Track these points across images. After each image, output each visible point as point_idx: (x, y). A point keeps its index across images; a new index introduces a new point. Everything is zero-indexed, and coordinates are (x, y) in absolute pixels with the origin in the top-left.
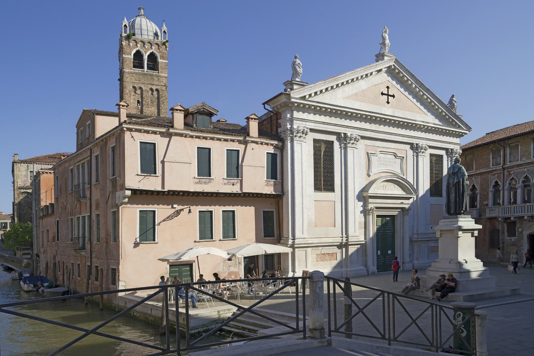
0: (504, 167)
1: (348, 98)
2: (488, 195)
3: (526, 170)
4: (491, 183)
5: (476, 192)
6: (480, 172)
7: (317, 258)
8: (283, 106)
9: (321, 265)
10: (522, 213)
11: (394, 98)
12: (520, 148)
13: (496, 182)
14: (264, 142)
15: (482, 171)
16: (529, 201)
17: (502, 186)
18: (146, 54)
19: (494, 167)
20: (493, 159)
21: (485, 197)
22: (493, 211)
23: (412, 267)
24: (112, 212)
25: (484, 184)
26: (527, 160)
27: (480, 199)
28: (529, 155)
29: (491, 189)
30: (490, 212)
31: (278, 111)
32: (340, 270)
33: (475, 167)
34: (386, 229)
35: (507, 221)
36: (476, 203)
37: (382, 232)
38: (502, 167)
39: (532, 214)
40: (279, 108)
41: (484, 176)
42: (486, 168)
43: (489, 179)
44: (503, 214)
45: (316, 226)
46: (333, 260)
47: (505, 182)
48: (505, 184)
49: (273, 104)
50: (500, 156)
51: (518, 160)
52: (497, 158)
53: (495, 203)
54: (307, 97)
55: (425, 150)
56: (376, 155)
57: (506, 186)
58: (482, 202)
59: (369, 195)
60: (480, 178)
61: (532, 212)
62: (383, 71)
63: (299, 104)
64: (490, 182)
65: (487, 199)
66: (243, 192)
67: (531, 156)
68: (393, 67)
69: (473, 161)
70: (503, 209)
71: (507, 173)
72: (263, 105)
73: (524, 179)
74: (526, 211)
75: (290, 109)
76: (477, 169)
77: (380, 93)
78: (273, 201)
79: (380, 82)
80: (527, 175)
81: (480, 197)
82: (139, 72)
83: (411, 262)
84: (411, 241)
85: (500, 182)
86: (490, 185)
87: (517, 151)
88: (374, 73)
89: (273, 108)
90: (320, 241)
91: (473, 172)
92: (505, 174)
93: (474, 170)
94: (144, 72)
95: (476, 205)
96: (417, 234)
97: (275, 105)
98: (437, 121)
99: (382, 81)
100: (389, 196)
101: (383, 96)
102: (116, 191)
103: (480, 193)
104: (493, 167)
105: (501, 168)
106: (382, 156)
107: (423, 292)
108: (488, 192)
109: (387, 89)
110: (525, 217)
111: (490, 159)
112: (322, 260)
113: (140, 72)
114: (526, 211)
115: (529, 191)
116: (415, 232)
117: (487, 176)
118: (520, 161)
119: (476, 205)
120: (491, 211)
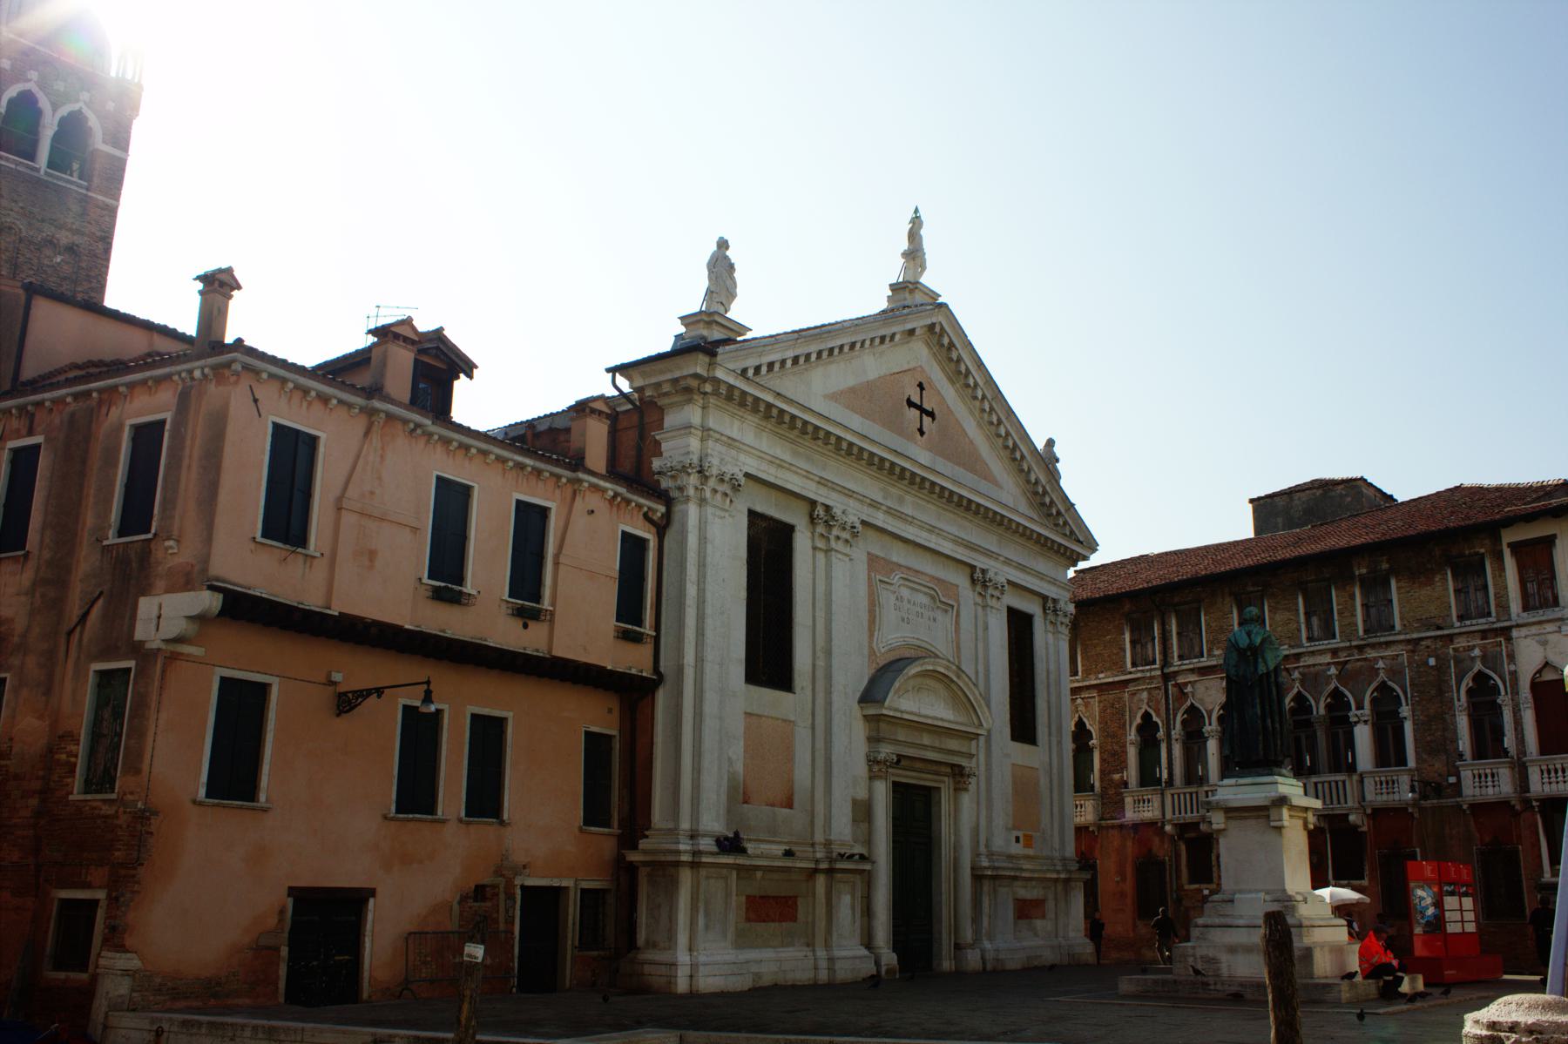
0: (1166, 671)
2: (1125, 752)
5: (1090, 743)
6: (1098, 682)
12: (1206, 621)
13: (1080, 724)
15: (1104, 678)
17: (1163, 728)
18: (54, 111)
20: (1135, 647)
21: (1115, 760)
22: (1144, 803)
23: (981, 961)
24: (95, 671)
25: (1111, 721)
27: (1101, 766)
29: (1132, 735)
30: (1136, 805)
31: (656, 400)
33: (1083, 666)
35: (1186, 836)
38: (1162, 672)
41: (1111, 695)
43: (1126, 705)
44: (1177, 812)
47: (1172, 717)
48: (1172, 722)
49: (644, 375)
50: (1154, 639)
51: (1202, 656)
52: (1146, 643)
53: (1148, 777)
54: (750, 373)
56: (892, 588)
57: (1174, 729)
58: (1109, 773)
59: (885, 712)
62: (917, 334)
63: (731, 387)
65: (1123, 766)
66: (553, 654)
68: (937, 329)
70: (1176, 796)
71: (1175, 689)
72: (611, 374)
76: (1087, 673)
77: (906, 398)
79: (906, 367)
81: (1103, 760)
82: (18, 168)
84: (978, 878)
85: (1158, 715)
86: (1128, 722)
88: (897, 337)
91: (1078, 681)
92: (1170, 692)
93: (1080, 673)
94: (36, 174)
98: (1023, 507)
99: (908, 363)
100: (929, 721)
101: (912, 409)
102: (145, 590)
103: (1101, 747)
104: (1134, 669)
105: (1159, 673)
107: (1209, 985)
108: (1125, 746)
109: (918, 389)
111: (1125, 645)
113: (20, 168)
116: (982, 849)
120: (1139, 803)
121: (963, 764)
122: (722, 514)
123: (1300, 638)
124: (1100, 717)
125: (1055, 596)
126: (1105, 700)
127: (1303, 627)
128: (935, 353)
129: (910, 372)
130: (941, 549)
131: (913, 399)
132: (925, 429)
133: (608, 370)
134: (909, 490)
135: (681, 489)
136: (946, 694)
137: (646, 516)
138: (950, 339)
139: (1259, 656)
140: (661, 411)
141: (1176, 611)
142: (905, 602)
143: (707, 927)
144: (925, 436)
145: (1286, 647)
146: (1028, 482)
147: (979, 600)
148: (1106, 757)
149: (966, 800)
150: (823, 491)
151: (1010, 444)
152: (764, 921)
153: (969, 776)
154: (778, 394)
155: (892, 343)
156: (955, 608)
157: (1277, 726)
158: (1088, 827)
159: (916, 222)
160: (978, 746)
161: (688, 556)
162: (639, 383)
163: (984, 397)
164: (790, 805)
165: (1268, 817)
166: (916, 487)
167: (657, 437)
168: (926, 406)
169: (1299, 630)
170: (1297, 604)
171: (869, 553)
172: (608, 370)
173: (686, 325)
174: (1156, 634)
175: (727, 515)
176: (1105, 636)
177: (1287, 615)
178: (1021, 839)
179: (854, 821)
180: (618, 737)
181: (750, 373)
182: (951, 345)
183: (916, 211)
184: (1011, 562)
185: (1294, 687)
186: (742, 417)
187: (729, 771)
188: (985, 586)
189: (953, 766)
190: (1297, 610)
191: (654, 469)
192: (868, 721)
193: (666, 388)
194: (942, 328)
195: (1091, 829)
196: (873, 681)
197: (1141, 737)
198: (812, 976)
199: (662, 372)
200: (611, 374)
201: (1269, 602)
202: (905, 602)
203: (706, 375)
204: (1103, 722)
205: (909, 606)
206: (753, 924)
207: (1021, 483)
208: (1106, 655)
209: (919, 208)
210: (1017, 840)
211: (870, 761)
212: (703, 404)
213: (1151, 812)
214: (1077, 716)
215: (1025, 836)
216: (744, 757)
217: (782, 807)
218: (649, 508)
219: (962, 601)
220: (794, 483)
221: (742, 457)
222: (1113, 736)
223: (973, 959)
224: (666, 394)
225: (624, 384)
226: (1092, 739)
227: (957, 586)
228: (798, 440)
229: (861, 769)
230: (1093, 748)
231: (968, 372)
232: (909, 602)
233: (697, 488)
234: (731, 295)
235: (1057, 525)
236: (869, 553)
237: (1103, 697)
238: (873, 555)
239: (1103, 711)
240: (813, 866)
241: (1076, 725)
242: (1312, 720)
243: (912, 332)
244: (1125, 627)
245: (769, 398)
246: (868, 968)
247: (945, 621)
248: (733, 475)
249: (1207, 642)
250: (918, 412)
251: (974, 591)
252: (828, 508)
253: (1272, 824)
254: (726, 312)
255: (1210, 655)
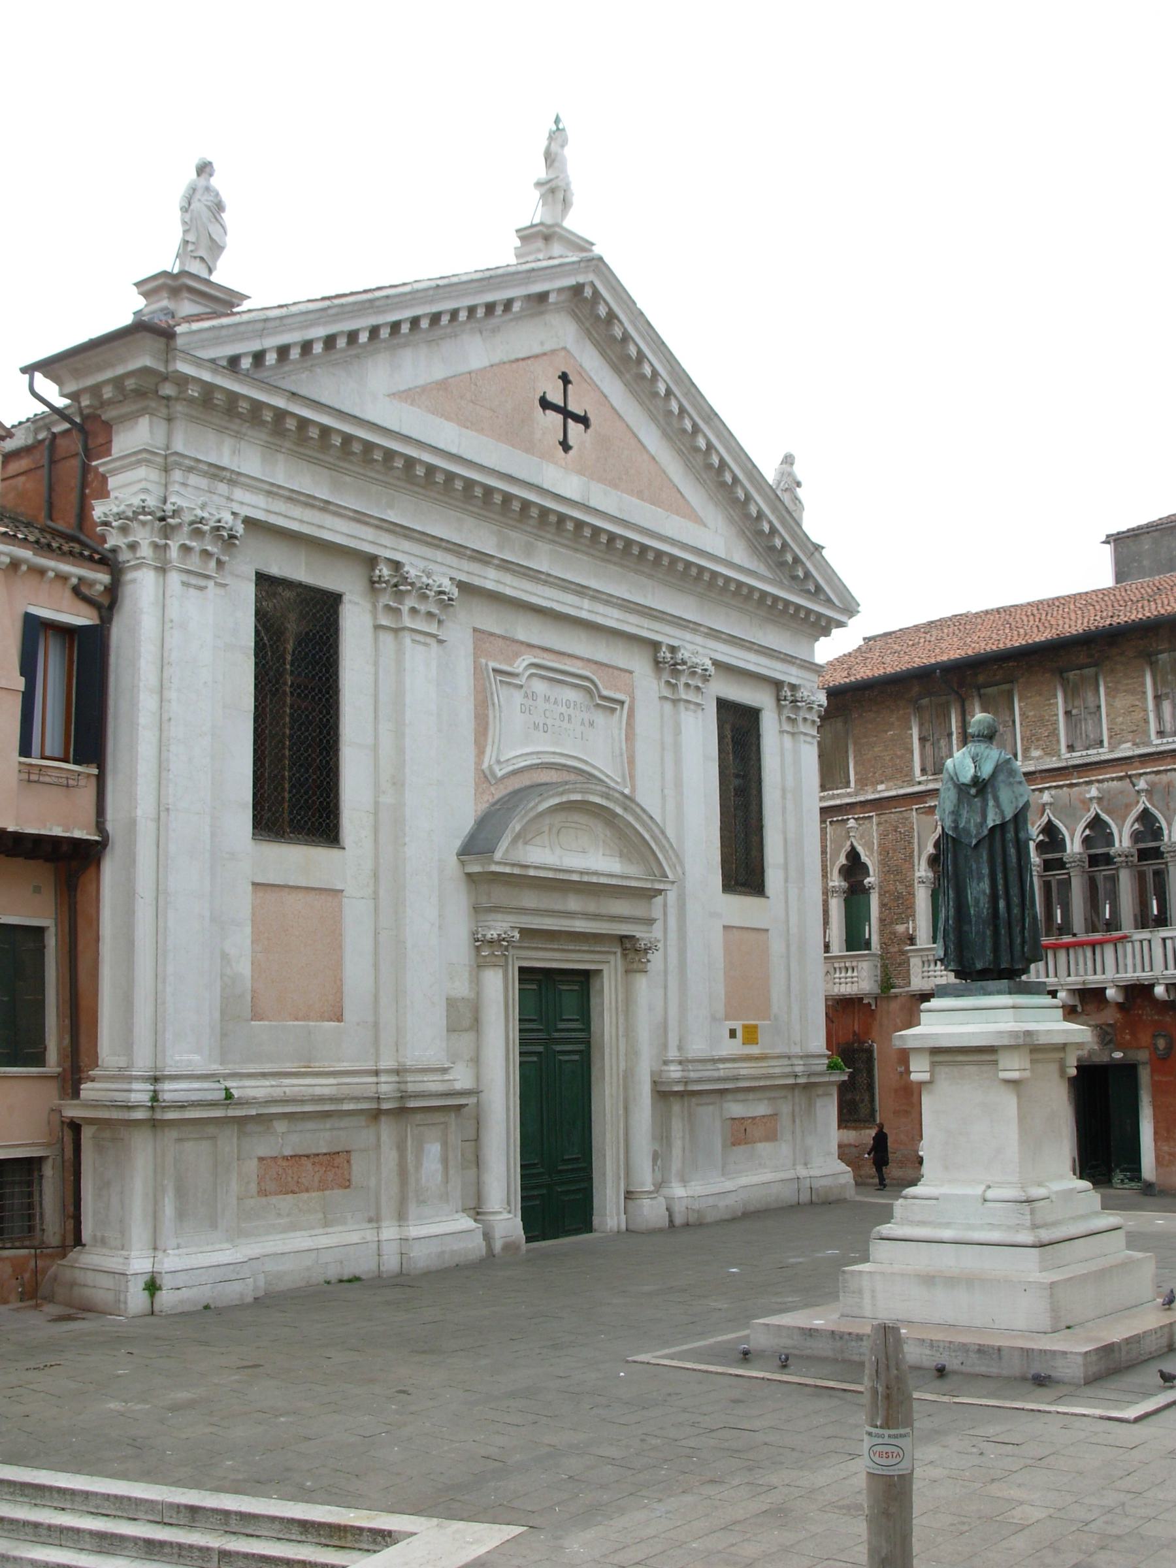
1: (408, 396)
2: (912, 895)
3: (1094, 792)
4: (919, 845)
6: (877, 796)
7: (261, 1179)
8: (132, 390)
9: (279, 1215)
10: (1143, 970)
11: (589, 431)
12: (1020, 708)
14: (26, 561)
15: (884, 790)
16: (1162, 921)
19: (930, 778)
25: (895, 850)
26: (1047, 759)
27: (881, 913)
28: (1050, 738)
31: (99, 412)
32: (370, 1235)
33: (856, 774)
34: (556, 1035)
36: (867, 928)
37: (540, 1049)
39: (1084, 983)
40: (105, 397)
42: (899, 783)
45: (256, 1016)
46: (332, 1189)
49: (77, 374)
50: (950, 735)
52: (939, 740)
54: (246, 363)
55: (706, 678)
58: (892, 923)
59: (495, 868)
60: (879, 824)
61: (1147, 968)
63: (209, 389)
64: (916, 840)
67: (1058, 741)
68: (588, 292)
69: (847, 752)
72: (27, 376)
73: (1087, 832)
74: (1130, 969)
75: (164, 411)
77: (538, 397)
78: (41, 873)
80: (1053, 818)
81: (883, 905)
83: (659, 1186)
86: (916, 853)
87: (1008, 719)
88: (516, 307)
89: (74, 396)
90: (277, 1093)
91: (849, 795)
93: (852, 784)
95: (867, 936)
96: (680, 1063)
97: (90, 381)
98: (740, 555)
99: (542, 344)
101: (548, 412)
103: (880, 887)
104: (924, 778)
106: (539, 687)
108: (912, 886)
109: (560, 382)
110: (1108, 992)
111: (912, 744)
112: (286, 1190)
114: (1130, 969)
115: (1160, 877)
117: (905, 814)
118: (1022, 761)
119: (867, 936)
121: (638, 935)
122: (202, 582)
123: (1146, 733)
124: (880, 845)
125: (794, 681)
126: (886, 821)
127: (1152, 717)
128: (587, 329)
129: (545, 358)
130: (600, 620)
131: (549, 398)
132: (571, 443)
133: (24, 370)
134: (557, 539)
135: (133, 547)
136: (608, 833)
137: (76, 591)
138: (610, 309)
139: (990, 796)
140: (108, 427)
141: (980, 696)
142: (540, 701)
143: (181, 1215)
144: (571, 452)
145: (1129, 745)
146: (747, 516)
147: (667, 693)
148: (886, 900)
149: (643, 986)
150: (386, 539)
151: (715, 460)
152: (293, 1192)
153: (646, 951)
154: (294, 394)
155: (508, 316)
156: (626, 706)
157: (1016, 911)
158: (862, 999)
159: (557, 134)
160: (665, 905)
161: (142, 649)
162: (72, 387)
163: (669, 392)
164: (340, 1019)
165: (995, 1062)
166: (553, 529)
167: (101, 470)
168: (573, 407)
169: (1146, 721)
170: (1143, 684)
171: (475, 630)
172: (24, 370)
173: (146, 295)
174: (954, 729)
175: (211, 584)
176: (886, 731)
177: (1130, 700)
178: (739, 1033)
179: (451, 1030)
180: (52, 930)
181: (246, 363)
182: (612, 316)
183: (557, 121)
184: (719, 635)
185: (1138, 802)
186: (238, 432)
187: (222, 975)
188: (675, 672)
189: (622, 939)
190: (1145, 693)
191: (95, 517)
192: (474, 882)
193: (108, 393)
194: (596, 293)
195: (865, 1001)
196: (482, 823)
197: (935, 873)
198: (374, 1267)
199: (100, 368)
200: (27, 376)
201: (1105, 683)
202: (540, 701)
203: (162, 369)
204: (885, 852)
205: (547, 706)
206: (274, 1200)
207: (736, 518)
208: (888, 758)
209: (561, 116)
210: (733, 1033)
211: (478, 941)
212: (169, 415)
213: (945, 978)
214: (849, 843)
215: (745, 1027)
216: (253, 951)
217: (322, 1018)
218: (80, 579)
219: (638, 694)
220: (337, 531)
221: (239, 494)
222: (897, 871)
223: (651, 1211)
224: (111, 402)
225: (48, 388)
226: (869, 876)
227: (631, 672)
228: (341, 464)
229: (460, 950)
230: (870, 888)
231: (641, 356)
232: (547, 699)
233: (156, 546)
234: (217, 248)
235: (794, 578)
236: (475, 630)
237: (884, 818)
238: (483, 632)
239: (883, 836)
240: (374, 1106)
241: (847, 857)
242: (1162, 849)
243: (543, 297)
244: (913, 718)
245: (280, 402)
246: (475, 1246)
247: (610, 727)
248: (219, 521)
249: (1022, 739)
250: (560, 417)
251: (660, 678)
252: (397, 565)
253: (1003, 1075)
254: (210, 271)
255: (1026, 757)
